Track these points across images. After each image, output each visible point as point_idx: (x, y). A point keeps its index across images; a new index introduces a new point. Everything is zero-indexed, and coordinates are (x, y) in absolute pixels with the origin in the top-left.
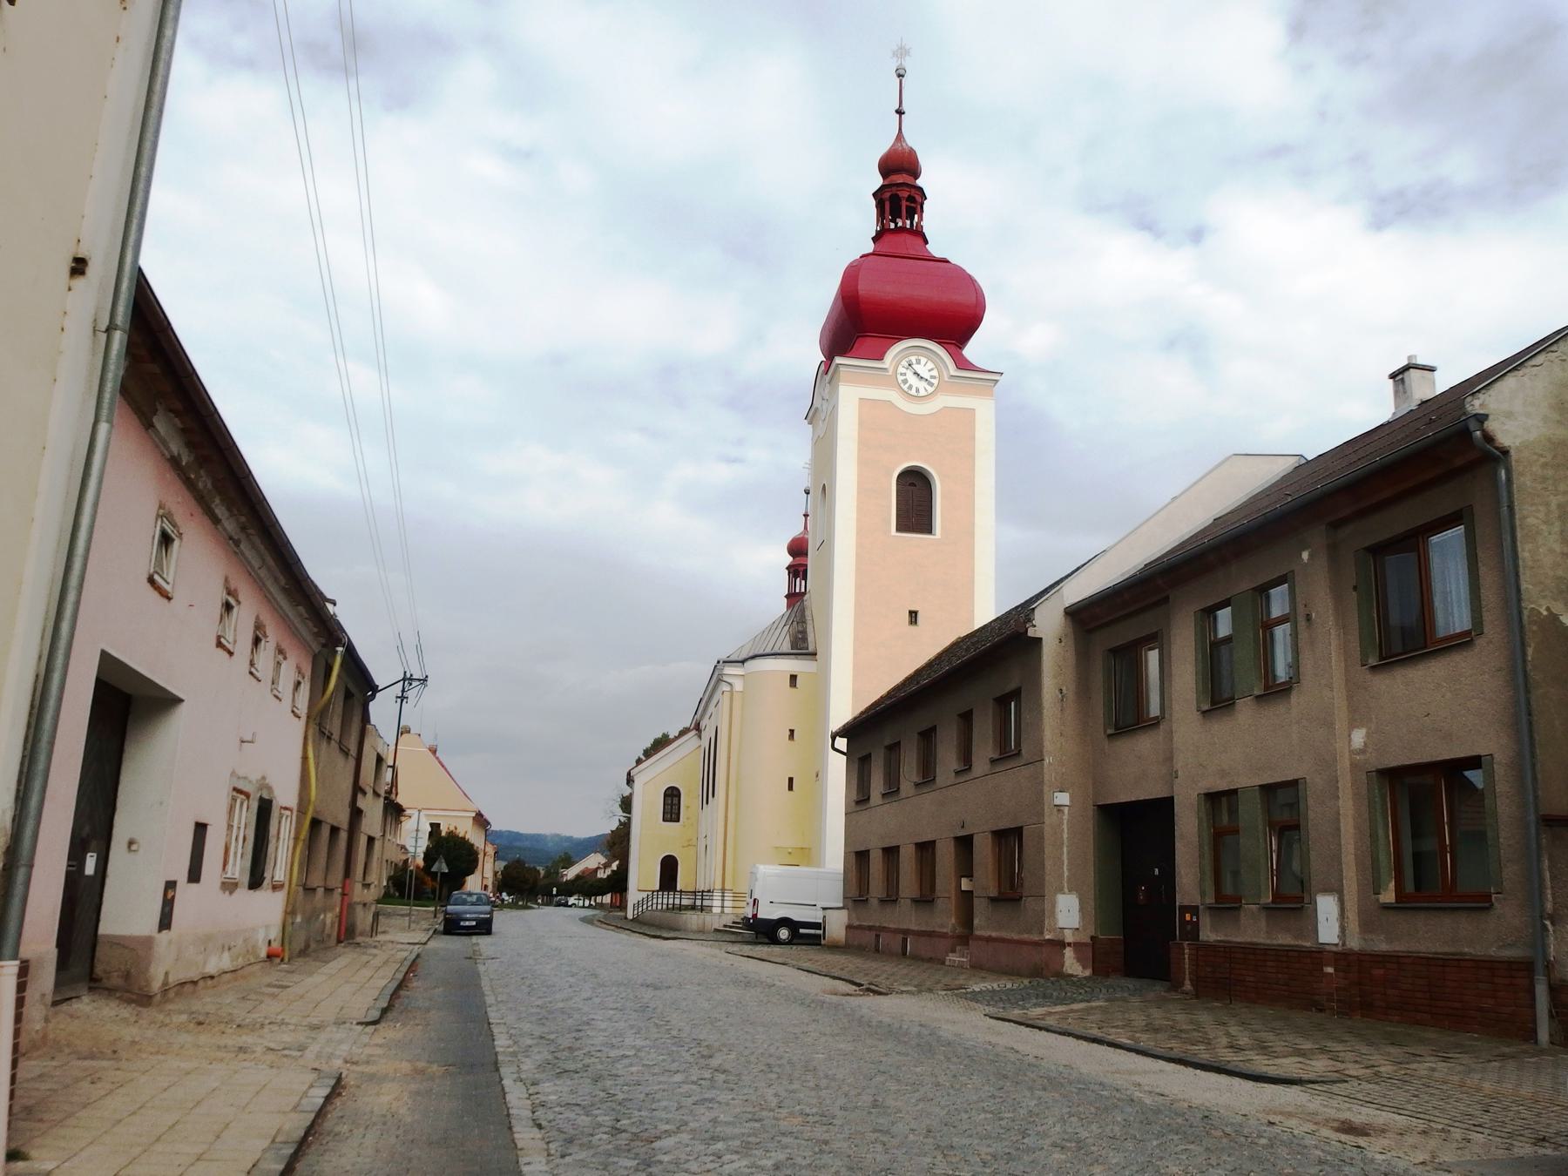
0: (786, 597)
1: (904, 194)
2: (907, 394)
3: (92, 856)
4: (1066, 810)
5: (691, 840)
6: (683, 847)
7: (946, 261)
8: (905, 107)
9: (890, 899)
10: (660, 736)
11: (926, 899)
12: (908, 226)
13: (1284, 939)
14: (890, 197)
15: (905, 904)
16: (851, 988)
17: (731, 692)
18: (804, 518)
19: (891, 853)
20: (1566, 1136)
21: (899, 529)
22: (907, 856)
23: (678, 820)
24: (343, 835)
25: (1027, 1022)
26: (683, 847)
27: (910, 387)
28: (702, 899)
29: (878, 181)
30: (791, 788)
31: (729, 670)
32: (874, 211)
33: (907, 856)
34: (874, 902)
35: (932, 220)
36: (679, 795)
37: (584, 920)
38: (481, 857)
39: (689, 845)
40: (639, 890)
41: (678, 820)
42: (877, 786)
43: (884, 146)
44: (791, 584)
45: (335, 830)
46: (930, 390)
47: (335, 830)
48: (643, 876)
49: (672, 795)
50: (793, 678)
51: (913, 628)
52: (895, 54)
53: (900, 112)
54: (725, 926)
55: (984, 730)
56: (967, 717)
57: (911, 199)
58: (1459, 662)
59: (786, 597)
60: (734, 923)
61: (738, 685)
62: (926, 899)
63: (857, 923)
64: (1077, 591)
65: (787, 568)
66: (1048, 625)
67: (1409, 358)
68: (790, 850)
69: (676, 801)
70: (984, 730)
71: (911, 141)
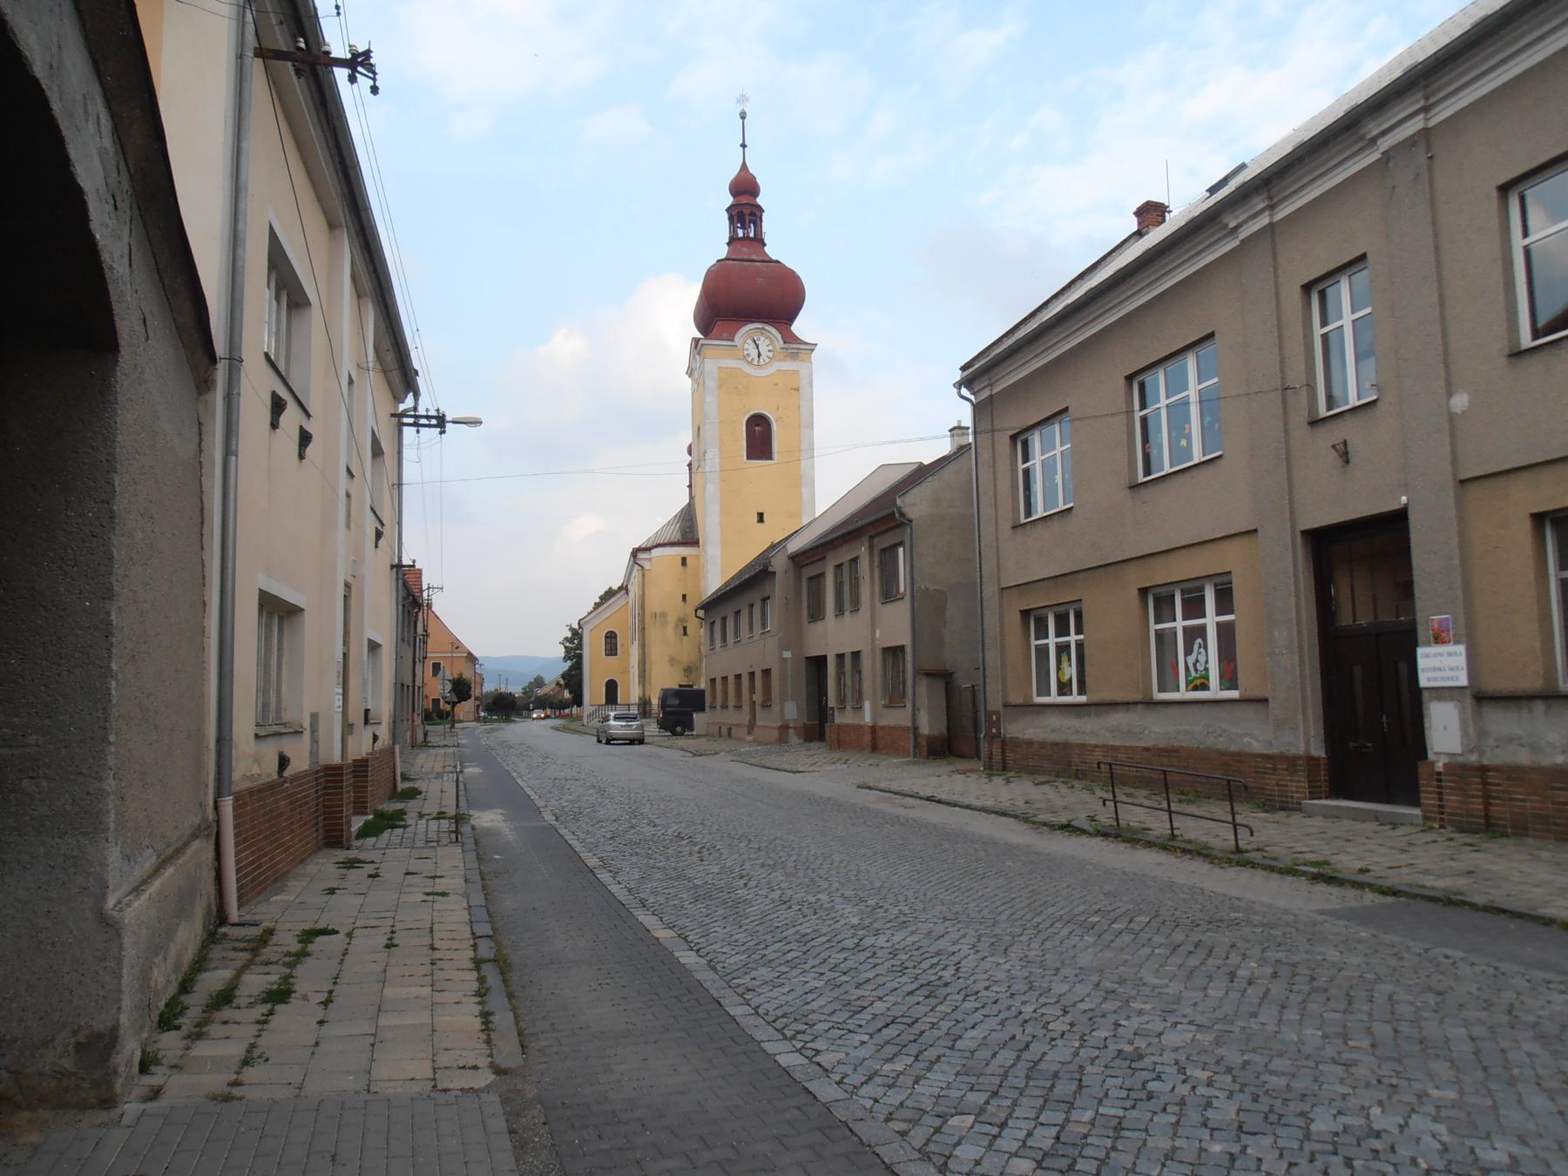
1: (747, 211)
4: (789, 661)
7: (777, 262)
8: (747, 143)
9: (725, 707)
11: (738, 707)
12: (752, 235)
13: (856, 722)
15: (731, 708)
16: (690, 755)
19: (752, 674)
20: (1566, 908)
21: (749, 457)
22: (731, 680)
23: (616, 655)
24: (411, 689)
25: (918, 802)
29: (729, 200)
30: (685, 634)
32: (727, 223)
33: (731, 680)
34: (718, 707)
35: (771, 228)
36: (616, 637)
37: (556, 729)
38: (472, 685)
41: (616, 655)
42: (718, 643)
43: (734, 171)
45: (408, 687)
47: (408, 687)
48: (593, 692)
49: (611, 637)
51: (761, 525)
52: (738, 101)
53: (744, 146)
55: (757, 611)
56: (724, 619)
57: (753, 214)
58: (900, 603)
62: (738, 707)
63: (711, 721)
64: (794, 546)
66: (779, 563)
67: (959, 421)
69: (613, 641)
70: (757, 611)
71: (753, 169)
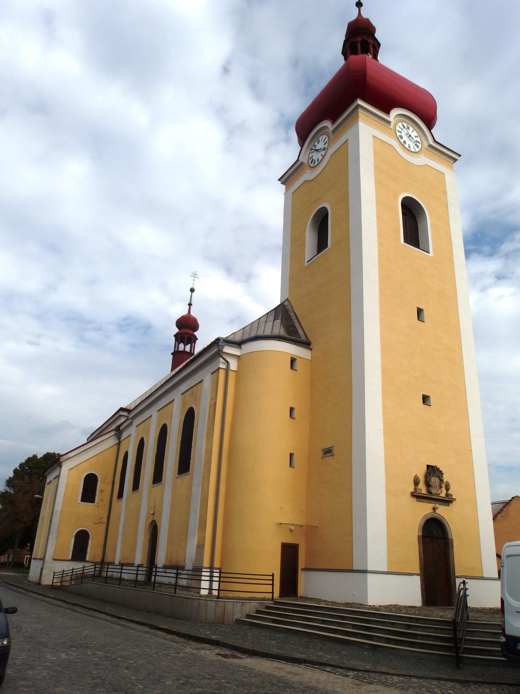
0: (172, 354)
2: (402, 145)
3: (163, 570)
5: (102, 518)
6: (95, 524)
10: (31, 456)
14: (362, 41)
17: (227, 370)
18: (188, 306)
26: (95, 524)
27: (405, 142)
28: (107, 571)
31: (227, 349)
39: (100, 522)
40: (54, 560)
44: (176, 346)
46: (417, 150)
50: (293, 361)
54: (249, 616)
59: (172, 354)
60: (258, 612)
61: (234, 365)
65: (175, 336)
68: (293, 528)
